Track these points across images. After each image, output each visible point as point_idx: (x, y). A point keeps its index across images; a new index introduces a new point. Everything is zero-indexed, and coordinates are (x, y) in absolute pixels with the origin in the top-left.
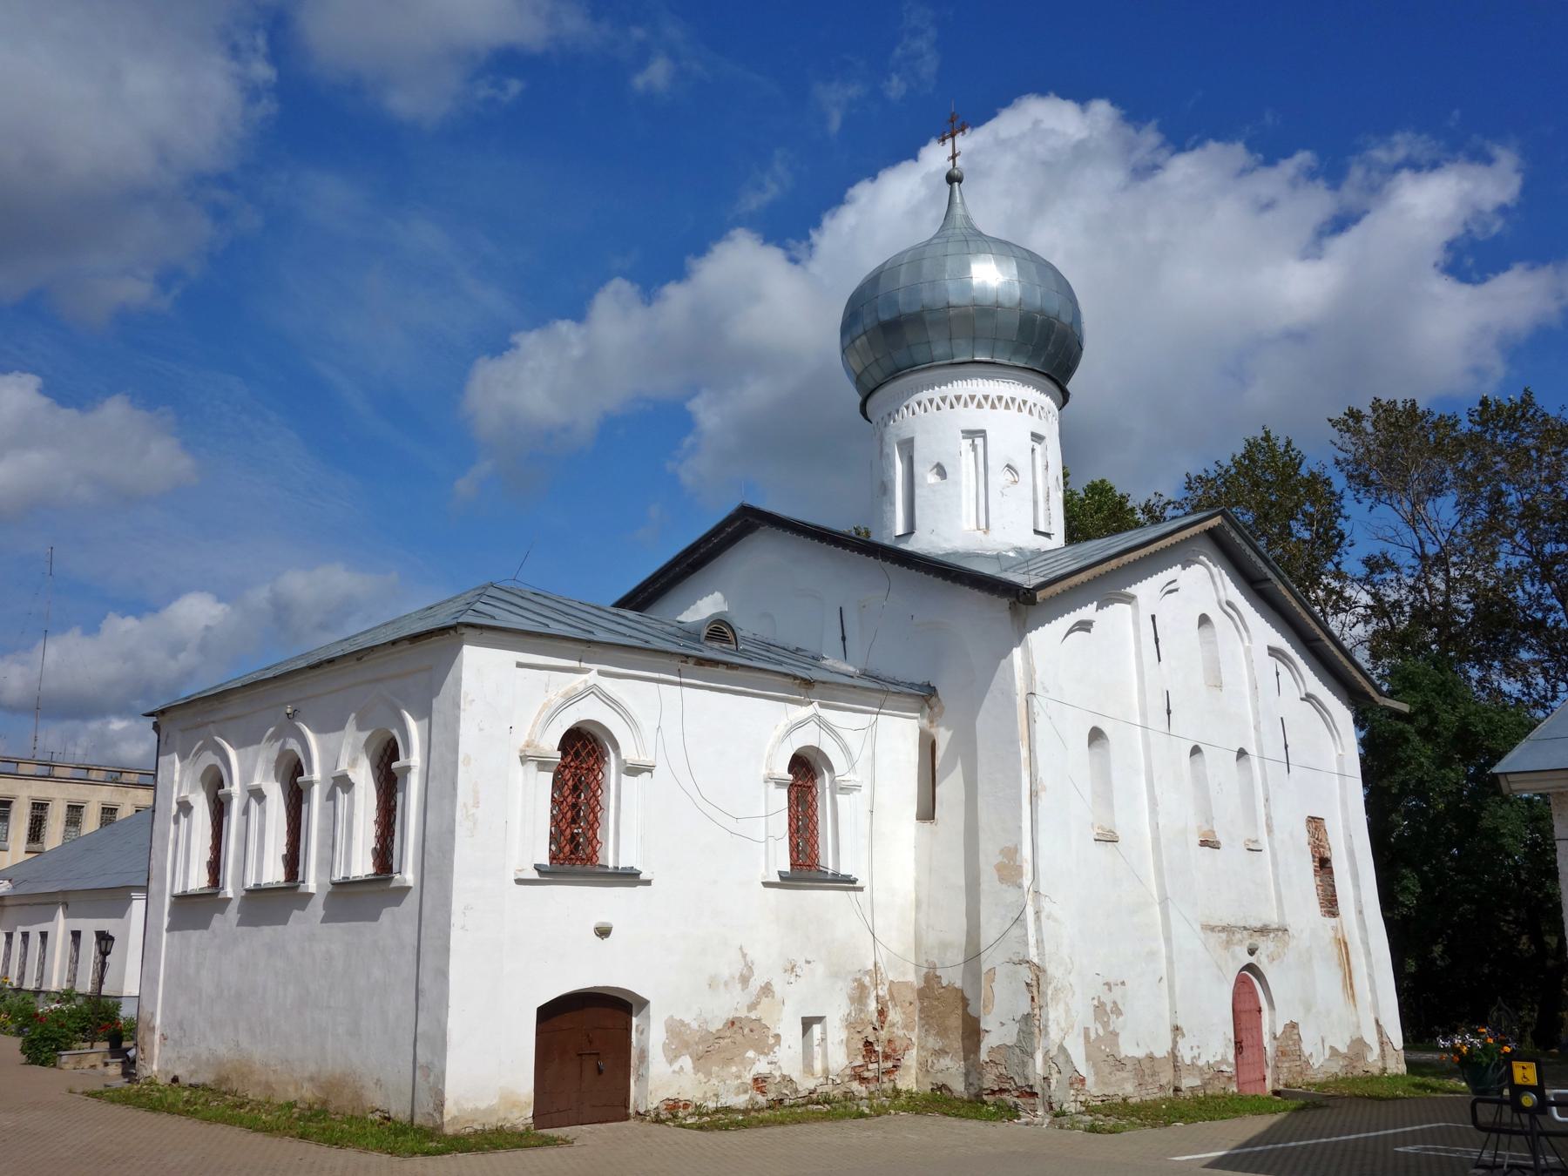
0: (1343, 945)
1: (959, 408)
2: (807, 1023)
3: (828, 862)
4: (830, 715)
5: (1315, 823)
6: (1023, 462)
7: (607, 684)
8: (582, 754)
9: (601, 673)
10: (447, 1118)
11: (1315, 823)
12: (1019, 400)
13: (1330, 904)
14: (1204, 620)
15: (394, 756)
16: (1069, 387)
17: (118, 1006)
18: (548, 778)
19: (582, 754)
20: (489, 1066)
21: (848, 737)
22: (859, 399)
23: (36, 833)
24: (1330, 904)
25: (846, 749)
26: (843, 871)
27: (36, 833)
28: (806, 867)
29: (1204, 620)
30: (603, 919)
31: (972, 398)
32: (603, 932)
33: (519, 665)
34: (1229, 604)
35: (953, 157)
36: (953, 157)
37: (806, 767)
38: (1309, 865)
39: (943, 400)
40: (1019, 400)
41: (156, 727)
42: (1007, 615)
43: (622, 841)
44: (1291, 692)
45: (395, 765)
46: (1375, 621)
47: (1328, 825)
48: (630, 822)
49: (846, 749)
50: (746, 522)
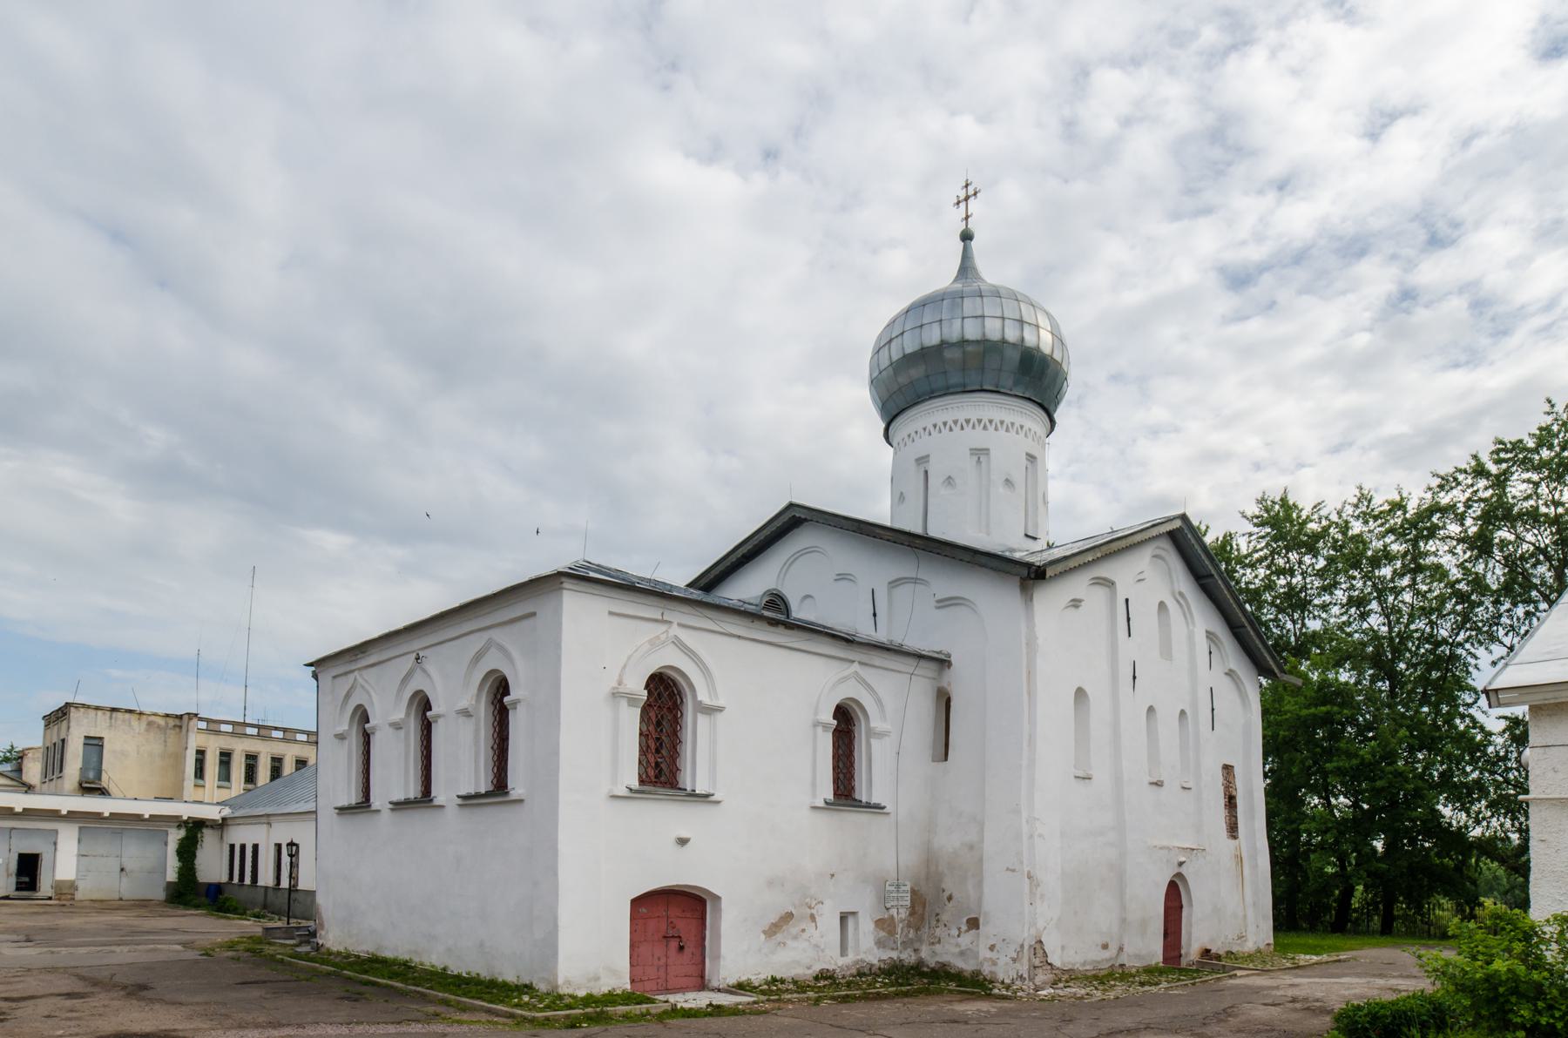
0: (1239, 859)
1: (968, 429)
2: (844, 918)
3: (862, 794)
4: (866, 673)
5: (1228, 769)
6: (1018, 477)
7: (687, 637)
8: (664, 701)
9: (680, 625)
10: (560, 982)
11: (1228, 769)
12: (1017, 425)
13: (1233, 830)
14: (1162, 605)
15: (506, 692)
16: (1056, 416)
17: (169, 884)
18: (636, 713)
19: (664, 701)
20: (591, 951)
21: (881, 692)
22: (883, 426)
23: (250, 776)
24: (1233, 830)
25: (879, 702)
26: (874, 800)
27: (250, 776)
28: (845, 791)
29: (1162, 605)
30: (684, 835)
31: (980, 421)
32: (683, 842)
33: (611, 613)
34: (1181, 594)
35: (967, 218)
36: (967, 218)
37: (846, 720)
38: (1222, 801)
39: (956, 422)
40: (1017, 425)
41: (315, 676)
42: (1018, 590)
43: (698, 770)
44: (1218, 669)
45: (506, 699)
46: (1316, 602)
47: (1237, 771)
48: (706, 751)
49: (879, 702)
50: (791, 522)
